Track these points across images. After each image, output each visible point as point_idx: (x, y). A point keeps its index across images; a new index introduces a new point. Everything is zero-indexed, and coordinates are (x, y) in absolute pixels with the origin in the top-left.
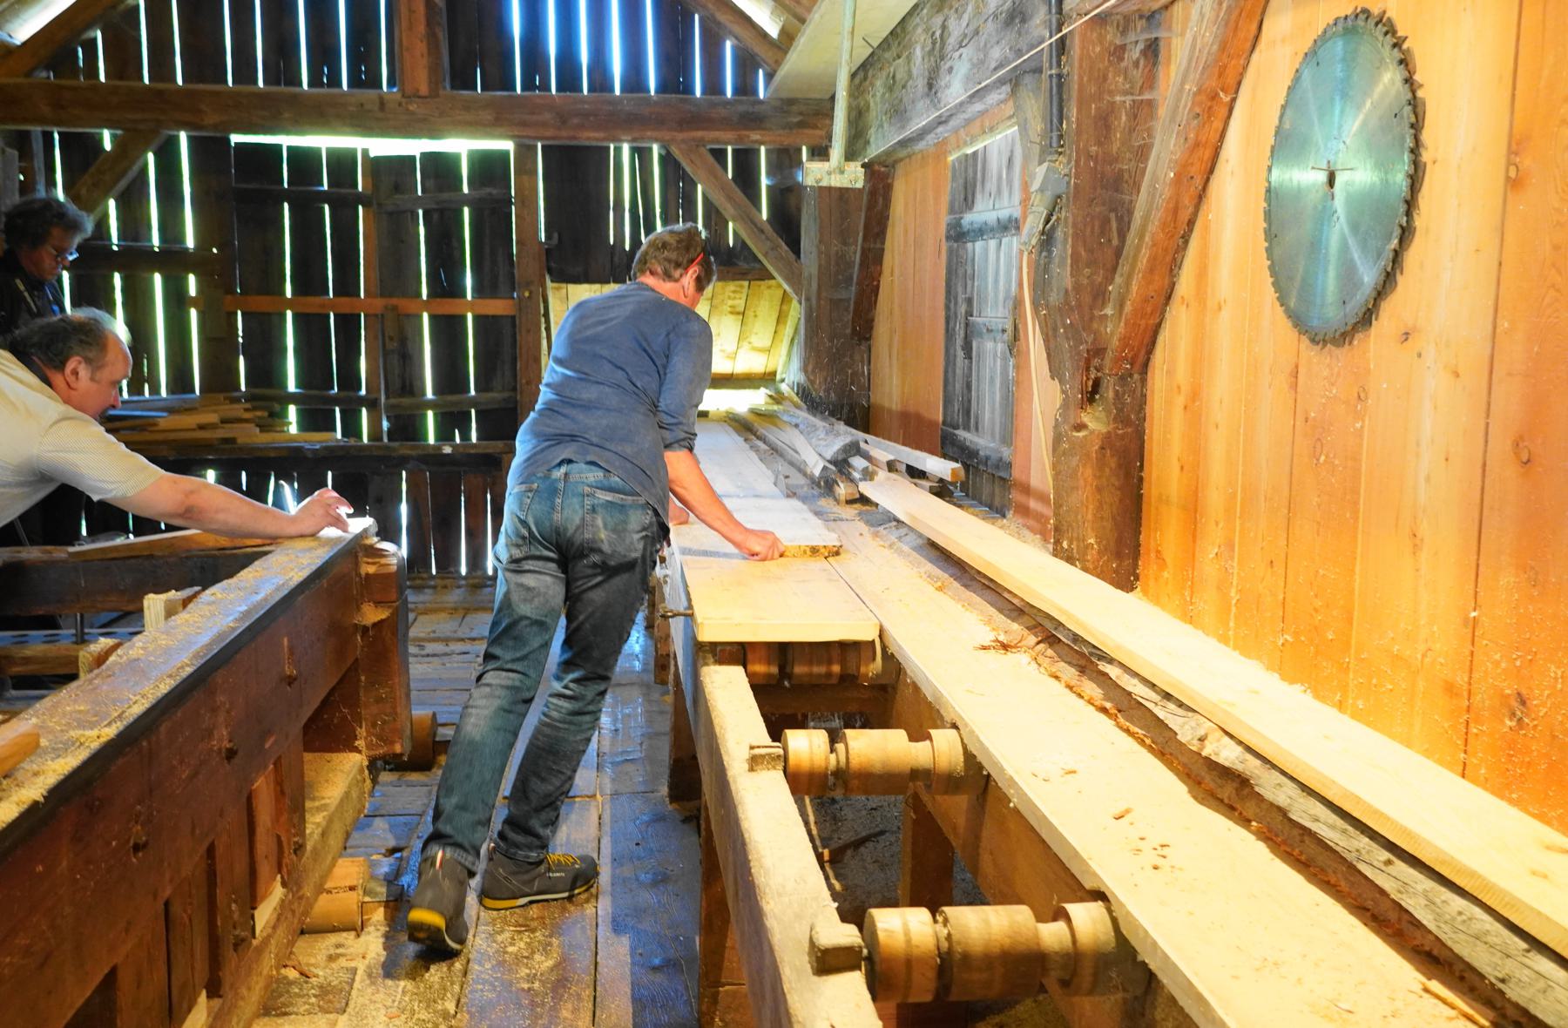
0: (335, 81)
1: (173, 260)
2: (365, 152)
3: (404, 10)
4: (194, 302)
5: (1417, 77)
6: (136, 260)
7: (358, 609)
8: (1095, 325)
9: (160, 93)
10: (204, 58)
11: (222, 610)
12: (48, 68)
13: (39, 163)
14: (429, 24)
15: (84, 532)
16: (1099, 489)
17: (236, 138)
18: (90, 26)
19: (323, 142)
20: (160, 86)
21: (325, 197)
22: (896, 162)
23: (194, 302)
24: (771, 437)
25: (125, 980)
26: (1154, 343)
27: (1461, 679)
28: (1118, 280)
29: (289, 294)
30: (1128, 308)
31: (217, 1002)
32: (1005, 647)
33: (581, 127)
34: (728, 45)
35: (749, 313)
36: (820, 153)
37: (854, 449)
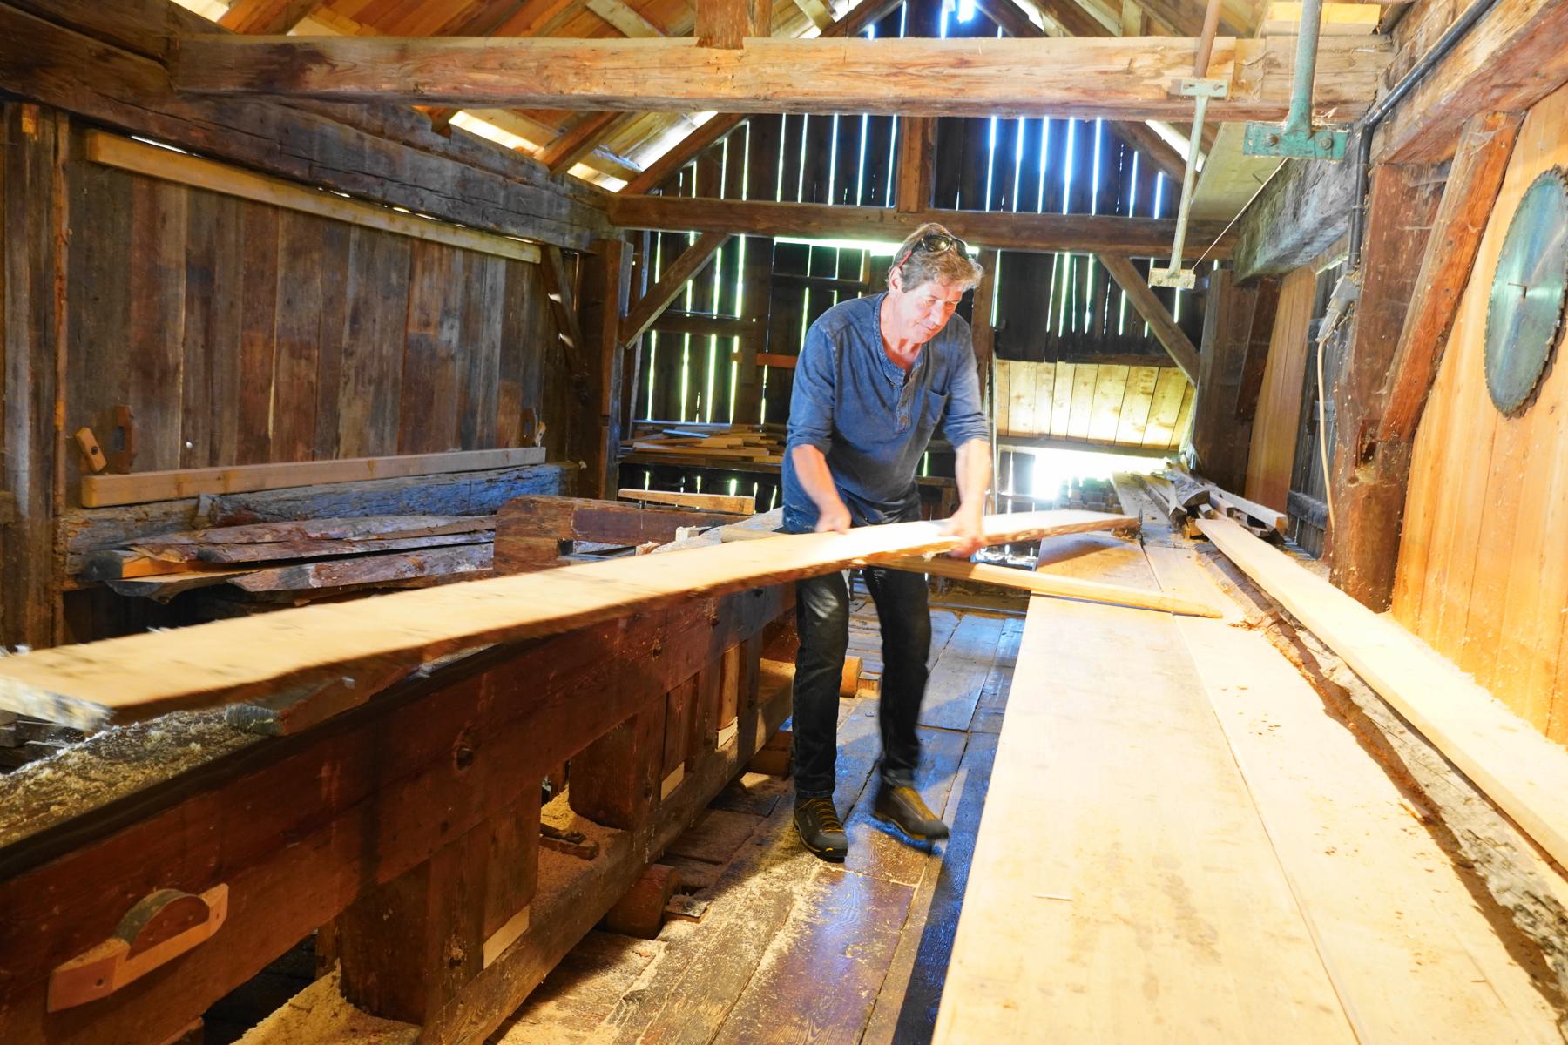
1: (725, 326)
2: (867, 253)
3: (905, 147)
4: (736, 357)
6: (701, 325)
8: (1371, 402)
9: (729, 206)
10: (762, 186)
12: (659, 188)
13: (646, 254)
14: (923, 159)
15: (647, 483)
16: (1363, 529)
17: (777, 240)
18: (689, 159)
19: (837, 244)
20: (729, 201)
21: (835, 285)
22: (1282, 276)
23: (736, 357)
26: (1418, 418)
27: (1553, 660)
28: (1392, 367)
30: (1396, 389)
32: (1250, 626)
33: (1030, 238)
36: (1164, 264)
37: (1205, 498)
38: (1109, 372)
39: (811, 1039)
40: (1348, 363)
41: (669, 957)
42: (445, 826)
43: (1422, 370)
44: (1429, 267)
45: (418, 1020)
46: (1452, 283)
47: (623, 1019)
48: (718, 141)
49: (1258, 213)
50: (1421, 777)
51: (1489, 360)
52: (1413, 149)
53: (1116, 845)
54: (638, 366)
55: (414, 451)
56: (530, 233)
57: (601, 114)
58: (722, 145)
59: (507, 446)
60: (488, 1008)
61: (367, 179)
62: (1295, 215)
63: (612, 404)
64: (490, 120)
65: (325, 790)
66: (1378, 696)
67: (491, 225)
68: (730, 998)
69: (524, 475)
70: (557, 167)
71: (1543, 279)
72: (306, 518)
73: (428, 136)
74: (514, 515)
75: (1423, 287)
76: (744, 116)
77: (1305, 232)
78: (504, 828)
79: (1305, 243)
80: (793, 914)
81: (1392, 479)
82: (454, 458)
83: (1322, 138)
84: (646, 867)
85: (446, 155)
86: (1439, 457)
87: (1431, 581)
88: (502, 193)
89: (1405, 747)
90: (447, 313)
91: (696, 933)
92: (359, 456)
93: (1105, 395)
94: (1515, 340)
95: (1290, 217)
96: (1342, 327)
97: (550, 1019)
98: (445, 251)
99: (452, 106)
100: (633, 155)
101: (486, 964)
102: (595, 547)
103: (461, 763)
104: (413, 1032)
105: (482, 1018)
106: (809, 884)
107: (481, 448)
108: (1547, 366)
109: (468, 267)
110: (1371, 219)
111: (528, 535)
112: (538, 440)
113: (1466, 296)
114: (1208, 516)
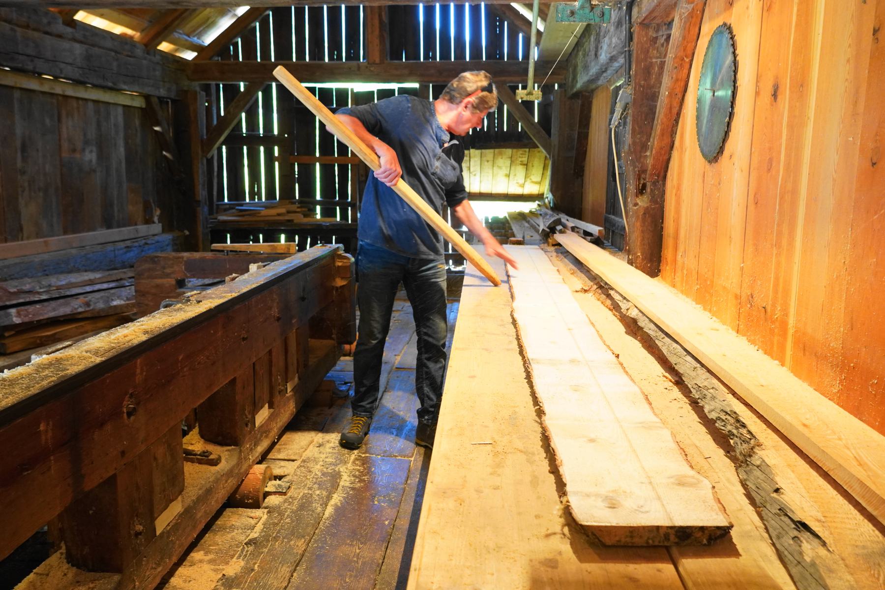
0: (340, 57)
1: (269, 140)
2: (352, 90)
4: (277, 159)
5: (737, 52)
6: (253, 140)
7: (334, 279)
11: (278, 268)
12: (218, 56)
13: (214, 98)
16: (643, 232)
18: (236, 36)
20: (265, 62)
22: (593, 91)
23: (277, 159)
24: (532, 221)
25: (239, 384)
29: (317, 155)
30: (654, 152)
31: (272, 410)
34: (521, 35)
35: (530, 165)
37: (558, 222)
38: (501, 154)
39: (358, 551)
40: (628, 139)
41: (270, 517)
42: (123, 453)
43: (667, 140)
44: (666, 82)
45: (119, 570)
46: (679, 90)
47: (246, 556)
48: (253, 25)
49: (577, 55)
50: (673, 360)
51: (699, 133)
52: (654, 15)
53: (515, 413)
54: (216, 169)
55: (74, 232)
56: (137, 88)
57: (175, 10)
58: (255, 27)
59: (136, 224)
60: (162, 558)
61: (21, 57)
62: (596, 55)
63: (201, 193)
64: (102, 16)
65: (43, 437)
66: (651, 321)
67: (110, 84)
68: (308, 535)
69: (149, 242)
70: (150, 45)
71: (722, 86)
72: (6, 280)
73: (60, 28)
74: (147, 266)
75: (664, 93)
76: (267, 9)
77: (602, 65)
78: (161, 451)
79: (603, 71)
80: (342, 483)
81: (656, 202)
82: (102, 234)
83: (598, 11)
84: (250, 467)
85: (74, 40)
86: (679, 188)
87: (679, 257)
88: (115, 64)
89: (665, 345)
90: (87, 142)
91: (285, 502)
92: (37, 238)
93: (500, 167)
94: (710, 121)
95: (593, 56)
96: (623, 118)
97: (201, 561)
98: (80, 102)
99: (74, 7)
100: (200, 35)
101: (158, 533)
102: (200, 282)
103: (129, 414)
104: (116, 578)
105: (159, 565)
106: (350, 465)
107: (119, 226)
108: (727, 133)
109: (97, 112)
110: (634, 55)
111: (156, 278)
112: (156, 219)
113: (686, 98)
114: (561, 232)
